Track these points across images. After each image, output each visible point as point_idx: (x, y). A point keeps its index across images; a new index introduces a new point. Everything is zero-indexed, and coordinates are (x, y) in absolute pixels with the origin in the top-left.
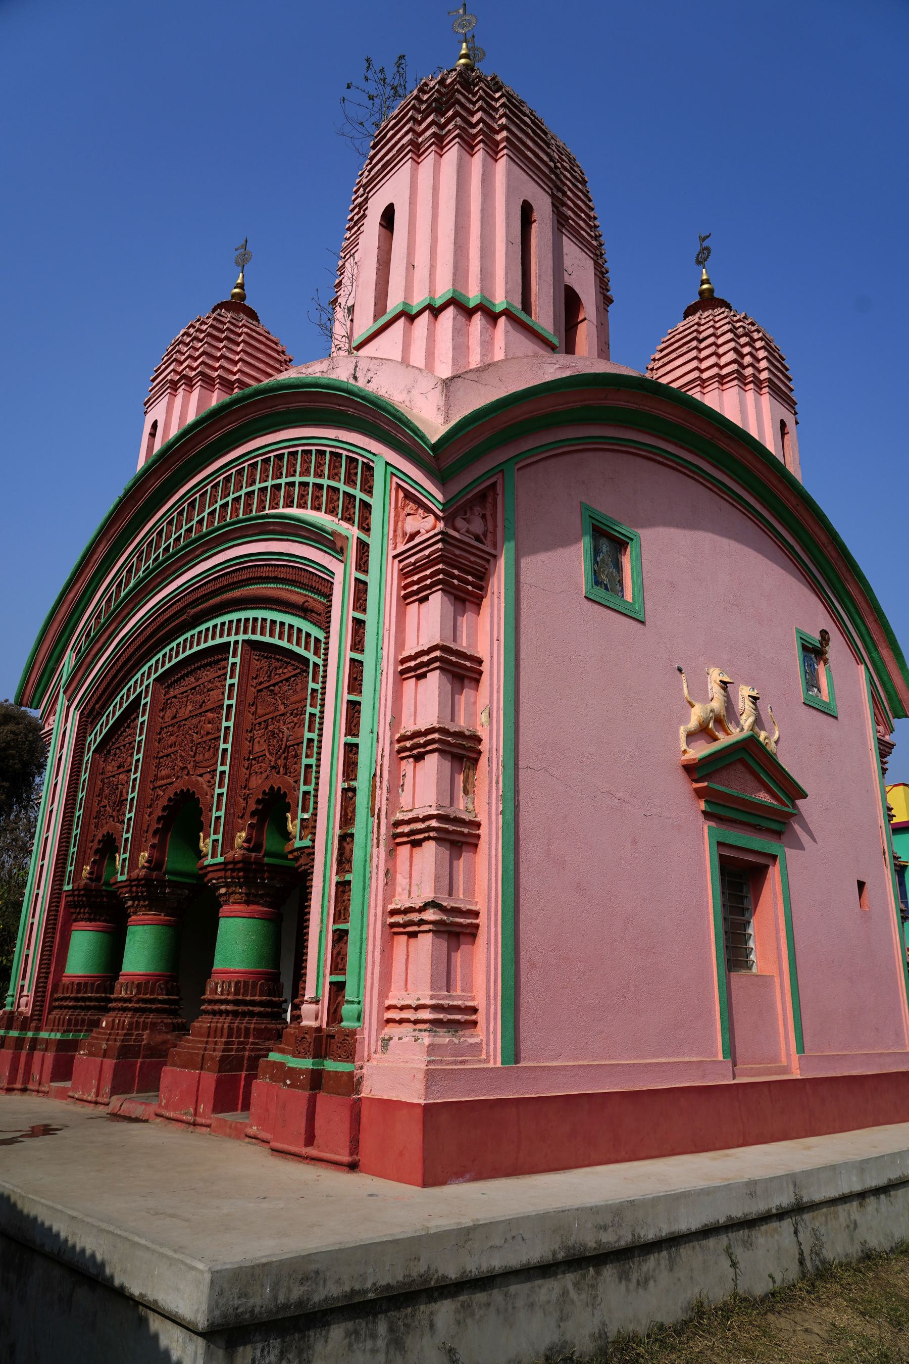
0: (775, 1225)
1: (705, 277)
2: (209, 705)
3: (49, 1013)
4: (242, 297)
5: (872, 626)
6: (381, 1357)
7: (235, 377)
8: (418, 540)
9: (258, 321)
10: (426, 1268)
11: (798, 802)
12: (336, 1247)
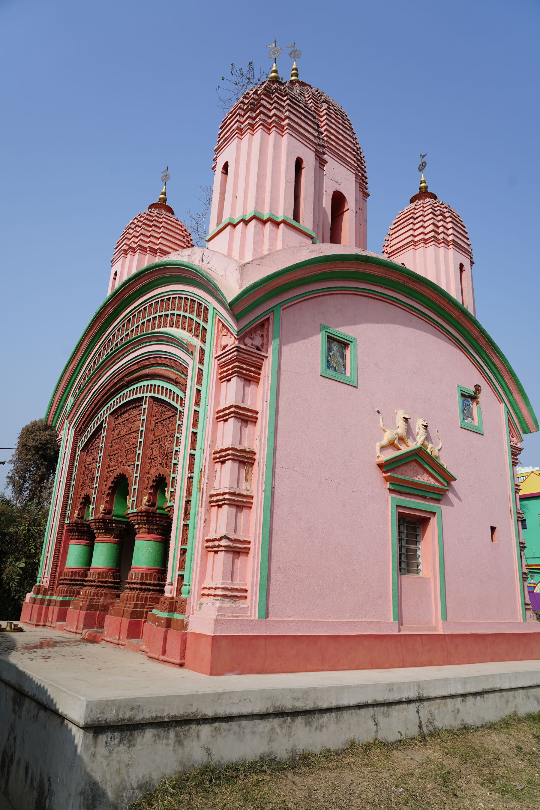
0: (404, 706)
1: (423, 179)
2: (134, 429)
3: (57, 587)
4: (165, 200)
5: (509, 381)
6: (171, 748)
7: (158, 247)
8: (227, 349)
9: (173, 214)
10: (196, 710)
11: (452, 483)
12: (150, 696)
